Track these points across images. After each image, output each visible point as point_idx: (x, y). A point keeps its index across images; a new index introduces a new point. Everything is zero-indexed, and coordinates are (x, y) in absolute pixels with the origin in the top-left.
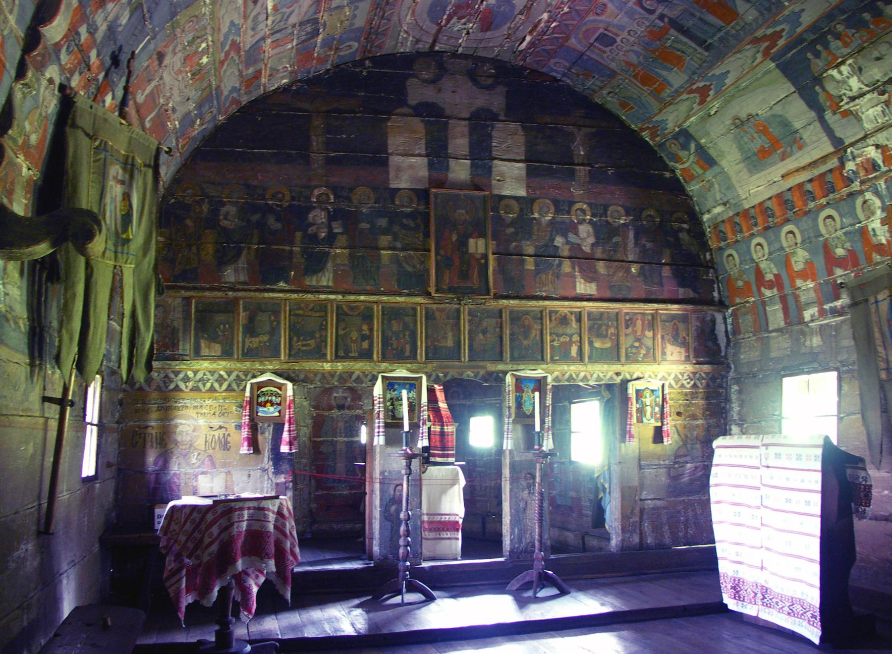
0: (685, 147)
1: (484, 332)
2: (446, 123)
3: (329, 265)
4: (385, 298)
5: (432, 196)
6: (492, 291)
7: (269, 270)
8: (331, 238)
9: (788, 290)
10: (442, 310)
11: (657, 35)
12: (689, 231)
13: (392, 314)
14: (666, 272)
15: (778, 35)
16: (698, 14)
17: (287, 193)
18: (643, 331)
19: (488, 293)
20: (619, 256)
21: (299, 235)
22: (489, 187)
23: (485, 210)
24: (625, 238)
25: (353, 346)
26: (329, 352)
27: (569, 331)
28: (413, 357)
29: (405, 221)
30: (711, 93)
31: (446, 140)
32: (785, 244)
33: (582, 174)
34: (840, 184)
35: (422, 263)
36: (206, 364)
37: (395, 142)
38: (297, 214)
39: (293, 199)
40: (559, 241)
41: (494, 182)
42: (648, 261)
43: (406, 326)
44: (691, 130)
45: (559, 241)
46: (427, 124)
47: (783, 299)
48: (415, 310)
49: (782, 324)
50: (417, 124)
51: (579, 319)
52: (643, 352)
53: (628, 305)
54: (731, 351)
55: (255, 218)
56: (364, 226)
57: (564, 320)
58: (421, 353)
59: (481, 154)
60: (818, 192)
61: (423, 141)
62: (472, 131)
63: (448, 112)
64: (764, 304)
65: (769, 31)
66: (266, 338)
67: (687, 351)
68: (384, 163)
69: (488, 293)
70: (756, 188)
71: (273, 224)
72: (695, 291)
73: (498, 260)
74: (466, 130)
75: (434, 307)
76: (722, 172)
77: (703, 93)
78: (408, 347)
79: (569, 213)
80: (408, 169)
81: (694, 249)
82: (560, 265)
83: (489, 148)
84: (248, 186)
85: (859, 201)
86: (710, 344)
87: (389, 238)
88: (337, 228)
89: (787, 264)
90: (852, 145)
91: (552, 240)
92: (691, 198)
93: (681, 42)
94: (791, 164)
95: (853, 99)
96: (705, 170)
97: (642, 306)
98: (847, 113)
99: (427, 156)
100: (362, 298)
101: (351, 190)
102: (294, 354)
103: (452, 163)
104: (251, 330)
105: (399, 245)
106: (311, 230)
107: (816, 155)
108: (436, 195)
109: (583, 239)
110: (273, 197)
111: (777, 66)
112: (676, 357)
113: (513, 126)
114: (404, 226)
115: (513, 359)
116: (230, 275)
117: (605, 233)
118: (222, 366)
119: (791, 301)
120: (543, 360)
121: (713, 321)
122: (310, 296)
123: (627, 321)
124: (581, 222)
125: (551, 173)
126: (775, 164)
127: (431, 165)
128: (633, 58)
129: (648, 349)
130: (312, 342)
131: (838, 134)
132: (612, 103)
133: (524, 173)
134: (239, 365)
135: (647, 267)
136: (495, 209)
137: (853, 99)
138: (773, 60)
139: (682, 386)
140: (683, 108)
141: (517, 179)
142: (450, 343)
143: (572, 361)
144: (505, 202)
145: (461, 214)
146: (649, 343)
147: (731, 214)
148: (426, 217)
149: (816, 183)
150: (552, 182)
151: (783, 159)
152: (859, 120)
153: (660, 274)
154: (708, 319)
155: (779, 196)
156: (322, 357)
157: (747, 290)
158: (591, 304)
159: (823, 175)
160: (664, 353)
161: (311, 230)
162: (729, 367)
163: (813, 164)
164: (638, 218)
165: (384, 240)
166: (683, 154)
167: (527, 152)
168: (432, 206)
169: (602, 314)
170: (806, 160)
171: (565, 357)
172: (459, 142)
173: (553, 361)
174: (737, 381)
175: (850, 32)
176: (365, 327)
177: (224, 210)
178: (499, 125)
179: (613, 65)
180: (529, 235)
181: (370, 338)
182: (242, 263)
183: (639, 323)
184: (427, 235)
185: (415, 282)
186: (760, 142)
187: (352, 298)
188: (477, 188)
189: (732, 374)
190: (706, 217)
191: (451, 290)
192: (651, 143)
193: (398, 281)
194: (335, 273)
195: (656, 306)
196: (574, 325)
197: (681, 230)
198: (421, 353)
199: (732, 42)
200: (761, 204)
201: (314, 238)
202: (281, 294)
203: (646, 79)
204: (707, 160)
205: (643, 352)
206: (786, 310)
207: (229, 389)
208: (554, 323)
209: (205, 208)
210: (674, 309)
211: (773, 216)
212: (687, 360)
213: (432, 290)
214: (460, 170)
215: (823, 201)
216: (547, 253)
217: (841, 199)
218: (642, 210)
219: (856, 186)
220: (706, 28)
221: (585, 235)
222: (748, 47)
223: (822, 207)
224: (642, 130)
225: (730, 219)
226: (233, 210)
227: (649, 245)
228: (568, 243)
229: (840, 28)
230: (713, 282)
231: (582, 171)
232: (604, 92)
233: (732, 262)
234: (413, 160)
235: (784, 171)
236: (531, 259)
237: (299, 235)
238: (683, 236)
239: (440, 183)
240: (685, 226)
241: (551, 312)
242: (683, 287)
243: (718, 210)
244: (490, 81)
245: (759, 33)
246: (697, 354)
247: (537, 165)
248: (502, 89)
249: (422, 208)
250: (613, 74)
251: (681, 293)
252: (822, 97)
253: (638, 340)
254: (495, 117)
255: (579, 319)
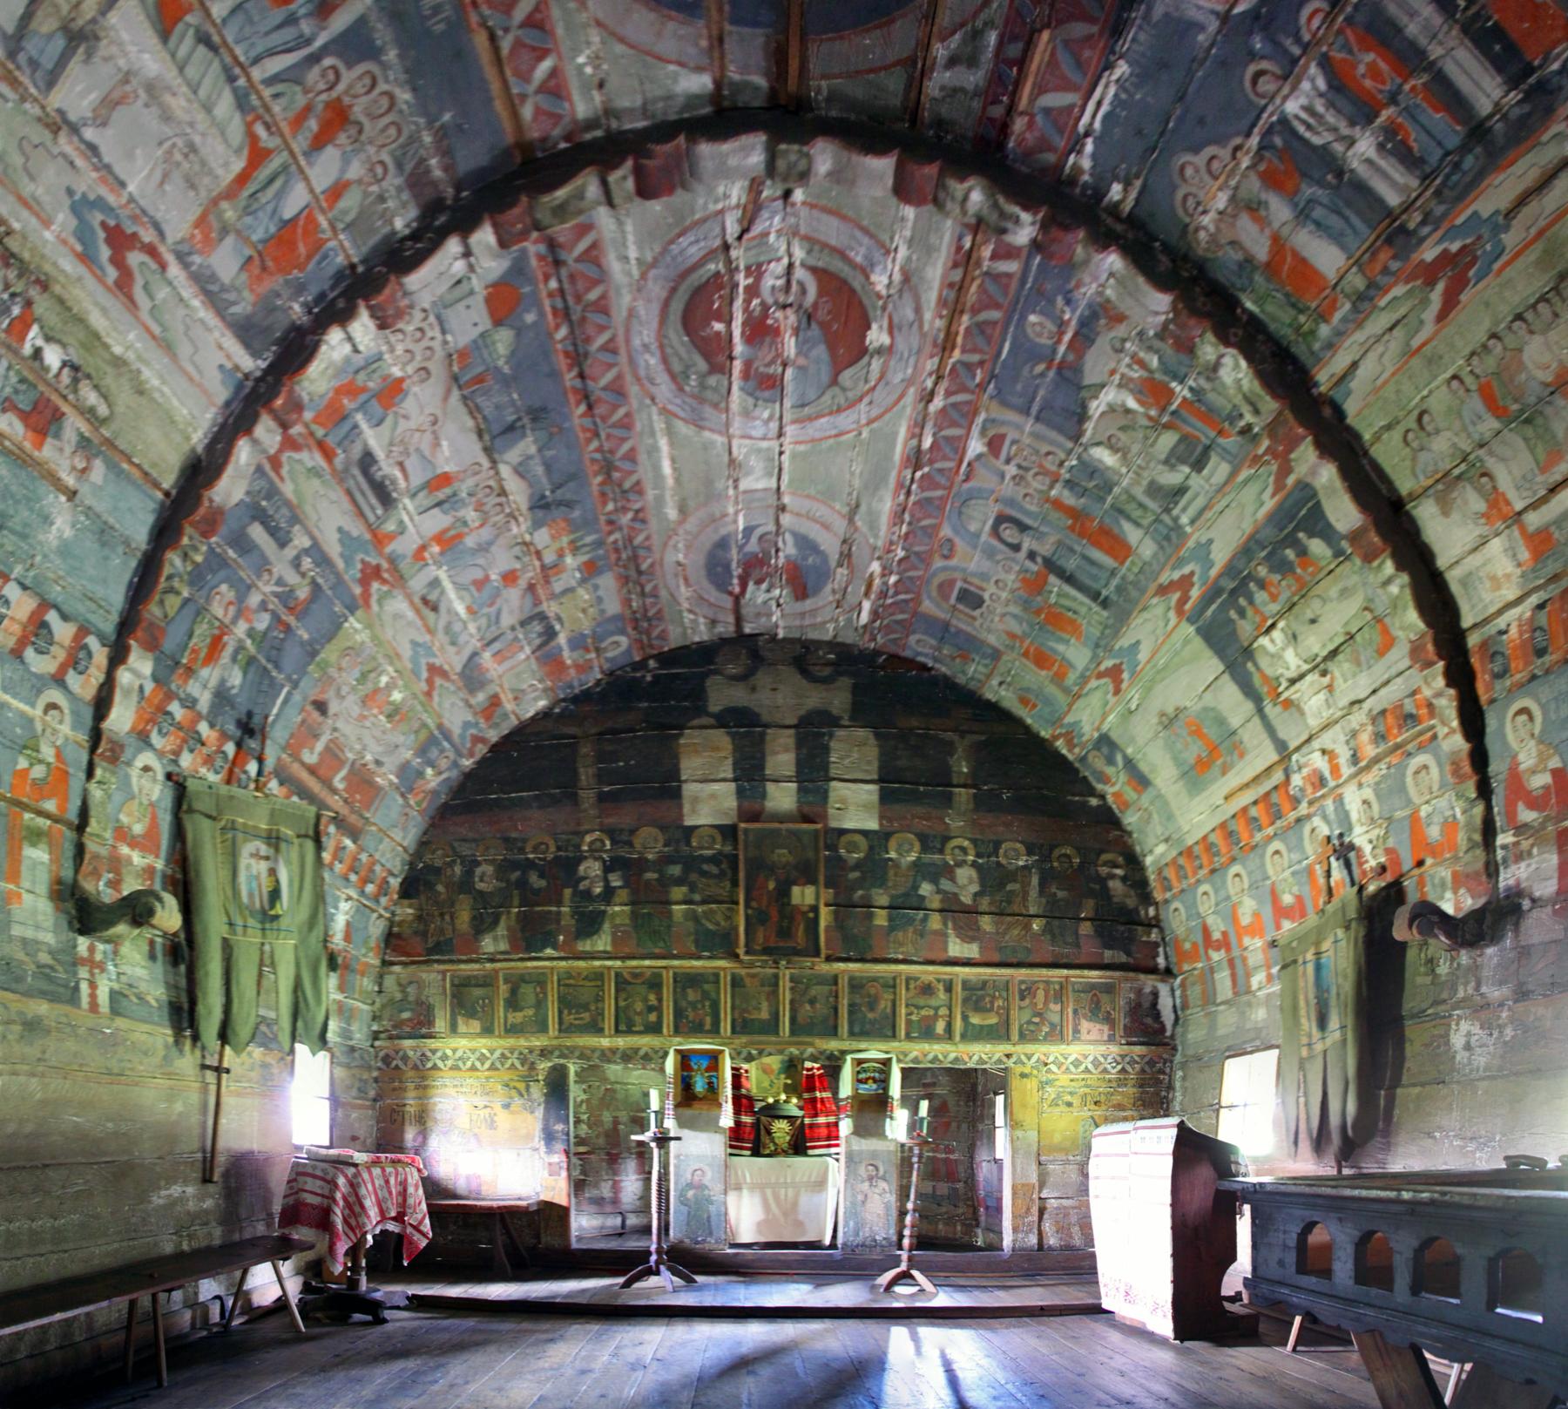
0: (1110, 761)
1: (812, 1002)
2: (763, 735)
3: (606, 926)
4: (676, 963)
5: (741, 837)
6: (824, 952)
7: (533, 935)
8: (609, 894)
9: (1236, 953)
10: (753, 976)
11: (1035, 585)
12: (1124, 879)
13: (687, 981)
14: (1086, 928)
15: (1185, 583)
16: (1078, 548)
17: (547, 839)
18: (1046, 1003)
19: (817, 954)
20: (1015, 908)
21: (568, 892)
22: (824, 817)
23: (817, 850)
24: (1026, 886)
25: (638, 1019)
26: (609, 1023)
27: (933, 1002)
28: (715, 1030)
29: (705, 867)
30: (1125, 676)
31: (763, 759)
32: (1232, 891)
33: (964, 798)
34: (1286, 806)
35: (728, 918)
36: (462, 1043)
37: (690, 766)
38: (565, 868)
39: (559, 849)
40: (926, 889)
41: (831, 811)
42: (1057, 914)
43: (706, 995)
44: (1114, 736)
45: (926, 889)
46: (733, 736)
47: (1231, 963)
48: (717, 976)
49: (1230, 994)
50: (722, 738)
51: (949, 988)
52: (1046, 1029)
53: (1023, 971)
54: (1179, 1030)
55: (515, 875)
56: (651, 876)
57: (927, 990)
58: (726, 1026)
59: (813, 773)
60: (1264, 820)
61: (730, 761)
62: (800, 743)
63: (765, 718)
64: (1212, 970)
65: (1176, 575)
66: (531, 1012)
67: (1112, 1028)
68: (676, 794)
69: (817, 954)
70: (1198, 815)
71: (536, 881)
72: (1128, 954)
73: (836, 913)
74: (791, 742)
75: (743, 972)
76: (1159, 796)
77: (1115, 674)
78: (708, 1020)
79: (941, 851)
80: (709, 800)
81: (1131, 902)
82: (925, 919)
83: (825, 766)
84: (506, 840)
85: (1307, 829)
86: (1149, 1021)
87: (684, 889)
88: (616, 881)
89: (1235, 919)
90: (1298, 749)
91: (916, 887)
92: (1130, 834)
93: (1066, 596)
94: (1234, 780)
95: (1293, 682)
96: (1140, 793)
97: (1044, 971)
98: (1288, 704)
99: (735, 780)
100: (647, 963)
101: (633, 832)
102: (564, 1029)
103: (770, 787)
104: (513, 1003)
105: (697, 897)
106: (582, 886)
107: (1260, 766)
108: (746, 831)
109: (963, 887)
110: (535, 849)
111: (1198, 631)
112: (1094, 1035)
113: (862, 733)
114: (704, 874)
115: (852, 1034)
116: (488, 944)
117: (994, 879)
118: (483, 1044)
119: (1238, 963)
120: (894, 1036)
121: (1155, 994)
122: (582, 964)
123: (1021, 992)
124: (960, 864)
125: (916, 798)
126: (1215, 780)
127: (740, 793)
128: (1016, 628)
129: (1053, 1026)
130: (586, 1015)
131: (1282, 735)
132: (1007, 698)
133: (875, 798)
134: (502, 1042)
135: (1056, 923)
136: (833, 847)
137: (1293, 682)
138: (1191, 621)
139: (1105, 1071)
140: (1095, 700)
141: (866, 807)
142: (764, 1015)
143: (937, 1039)
144: (848, 837)
145: (782, 855)
146: (1056, 1019)
147: (1174, 853)
148: (733, 861)
149: (1261, 805)
150: (920, 810)
151: (1224, 773)
152: (1302, 713)
153: (1076, 933)
154: (1148, 990)
155: (1223, 825)
156: (599, 1031)
157: (1193, 956)
158: (967, 970)
159: (1267, 794)
160: (1076, 1031)
161: (582, 886)
162: (1175, 1049)
163: (1256, 779)
164: (1046, 858)
165: (678, 892)
166: (1110, 771)
167: (881, 768)
168: (741, 846)
169: (985, 983)
170: (1249, 774)
171: (927, 1034)
172: (782, 758)
173: (908, 1037)
174: (1183, 1066)
175: (1276, 577)
176: (652, 997)
177: (478, 871)
178: (840, 733)
179: (992, 639)
180: (881, 882)
181: (658, 1009)
182: (501, 930)
183: (1041, 994)
184: (735, 883)
185: (723, 943)
186: (1195, 750)
187: (634, 963)
188: (807, 819)
189: (1178, 1058)
190: (1149, 860)
191: (767, 951)
192: (1070, 757)
193: (696, 942)
194: (614, 935)
195: (1065, 972)
196: (942, 995)
197: (1113, 876)
198: (726, 1026)
199: (1134, 593)
200: (1205, 838)
201: (587, 895)
202: (549, 963)
203: (1042, 659)
204: (1141, 781)
205: (1046, 1029)
206: (1234, 976)
207: (493, 1068)
208: (912, 992)
209: (458, 869)
210: (1094, 975)
211: (1217, 854)
212: (1111, 1039)
213: (741, 951)
214: (782, 797)
215: (1270, 831)
216: (906, 904)
217: (1289, 828)
218: (1052, 848)
219: (1303, 809)
220: (1094, 571)
221: (966, 882)
222: (1155, 601)
223: (1270, 839)
224: (1056, 738)
225: (1174, 861)
226: (489, 869)
227: (1061, 894)
228: (939, 891)
229: (1262, 571)
230: (1156, 945)
231: (963, 795)
232: (995, 682)
233: (1178, 920)
234: (716, 787)
235: (1225, 791)
236: (884, 913)
237: (568, 892)
238: (1116, 886)
239: (754, 816)
240: (1119, 872)
241: (908, 980)
242: (1110, 948)
243: (1161, 849)
244: (827, 671)
245: (1164, 578)
246: (1128, 1032)
247: (894, 787)
248: (846, 682)
249: (728, 849)
250: (996, 655)
251: (1108, 955)
252: (1257, 680)
253: (1039, 1015)
254: (834, 722)
255: (949, 988)
